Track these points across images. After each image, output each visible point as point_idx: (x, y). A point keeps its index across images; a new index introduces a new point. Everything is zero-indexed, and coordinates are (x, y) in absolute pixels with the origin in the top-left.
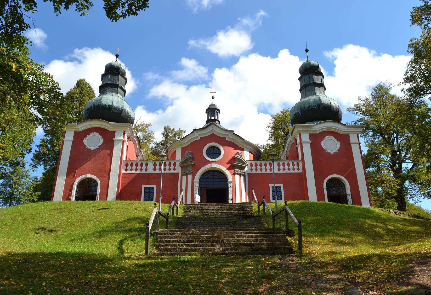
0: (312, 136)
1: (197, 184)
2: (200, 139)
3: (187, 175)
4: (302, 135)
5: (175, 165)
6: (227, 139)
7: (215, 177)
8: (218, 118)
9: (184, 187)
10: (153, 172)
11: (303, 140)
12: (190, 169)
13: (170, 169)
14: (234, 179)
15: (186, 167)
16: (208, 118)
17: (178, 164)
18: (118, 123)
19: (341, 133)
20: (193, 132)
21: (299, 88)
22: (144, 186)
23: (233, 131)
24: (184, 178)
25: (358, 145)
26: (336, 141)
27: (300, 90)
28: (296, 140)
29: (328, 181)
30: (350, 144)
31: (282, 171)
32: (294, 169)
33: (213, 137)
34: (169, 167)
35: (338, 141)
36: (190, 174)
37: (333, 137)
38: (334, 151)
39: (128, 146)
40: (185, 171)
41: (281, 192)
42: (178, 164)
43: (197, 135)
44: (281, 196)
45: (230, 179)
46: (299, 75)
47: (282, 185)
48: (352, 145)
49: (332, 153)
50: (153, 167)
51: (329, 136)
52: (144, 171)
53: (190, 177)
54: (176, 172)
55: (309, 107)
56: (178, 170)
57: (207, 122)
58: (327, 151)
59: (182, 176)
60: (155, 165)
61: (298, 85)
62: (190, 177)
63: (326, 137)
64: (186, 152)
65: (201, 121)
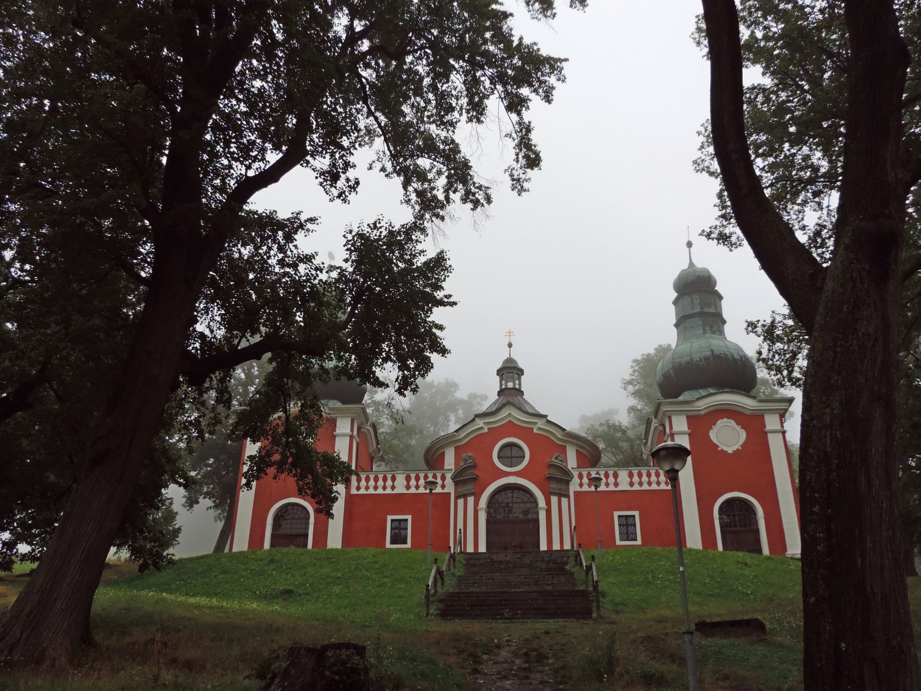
0: (693, 420)
1: (482, 517)
2: (486, 430)
3: (465, 496)
4: (674, 419)
5: (443, 478)
6: (535, 431)
7: (515, 500)
8: (520, 384)
9: (460, 525)
10: (405, 491)
11: (675, 429)
12: (470, 487)
13: (367, 488)
14: (548, 503)
15: (465, 482)
16: (501, 385)
17: (449, 476)
18: (344, 403)
19: (748, 412)
20: (473, 420)
21: (675, 322)
22: (390, 518)
23: (546, 416)
24: (461, 502)
25: (781, 435)
26: (738, 428)
27: (677, 325)
28: (664, 427)
29: (723, 504)
30: (766, 434)
31: (636, 487)
32: (650, 484)
33: (511, 428)
34: (391, 483)
35: (742, 428)
36: (470, 494)
37: (733, 422)
38: (735, 448)
39: (358, 444)
40: (461, 489)
41: (635, 525)
42: (449, 476)
43: (481, 425)
44: (635, 533)
45: (542, 503)
46: (675, 295)
47: (636, 513)
48: (770, 436)
49: (730, 450)
50: (405, 483)
51: (725, 420)
52: (389, 491)
53: (471, 500)
54: (446, 491)
55: (688, 363)
56: (450, 488)
57: (500, 393)
58: (722, 447)
59: (457, 498)
60: (408, 479)
61: (671, 315)
62: (471, 500)
63: (719, 422)
64: (464, 456)
65: (490, 388)
